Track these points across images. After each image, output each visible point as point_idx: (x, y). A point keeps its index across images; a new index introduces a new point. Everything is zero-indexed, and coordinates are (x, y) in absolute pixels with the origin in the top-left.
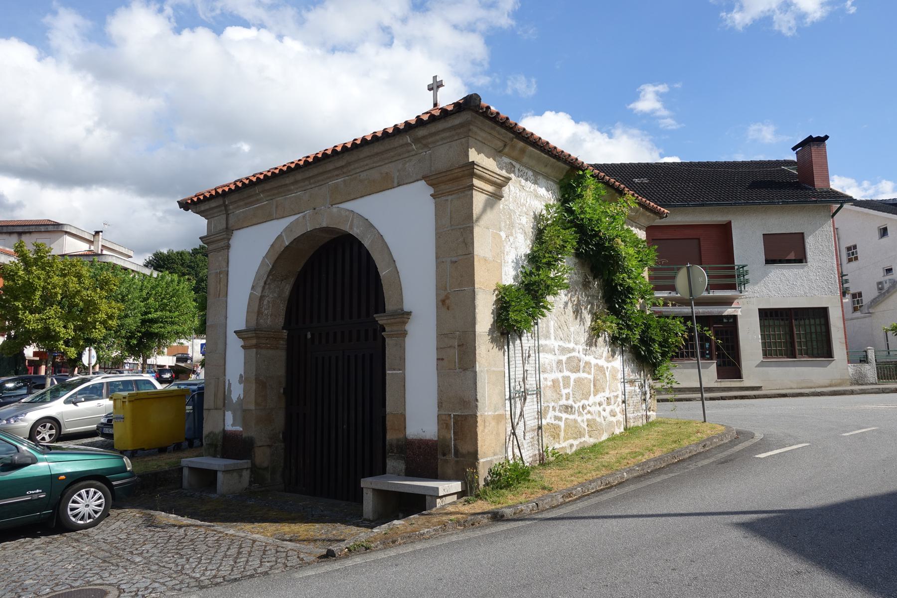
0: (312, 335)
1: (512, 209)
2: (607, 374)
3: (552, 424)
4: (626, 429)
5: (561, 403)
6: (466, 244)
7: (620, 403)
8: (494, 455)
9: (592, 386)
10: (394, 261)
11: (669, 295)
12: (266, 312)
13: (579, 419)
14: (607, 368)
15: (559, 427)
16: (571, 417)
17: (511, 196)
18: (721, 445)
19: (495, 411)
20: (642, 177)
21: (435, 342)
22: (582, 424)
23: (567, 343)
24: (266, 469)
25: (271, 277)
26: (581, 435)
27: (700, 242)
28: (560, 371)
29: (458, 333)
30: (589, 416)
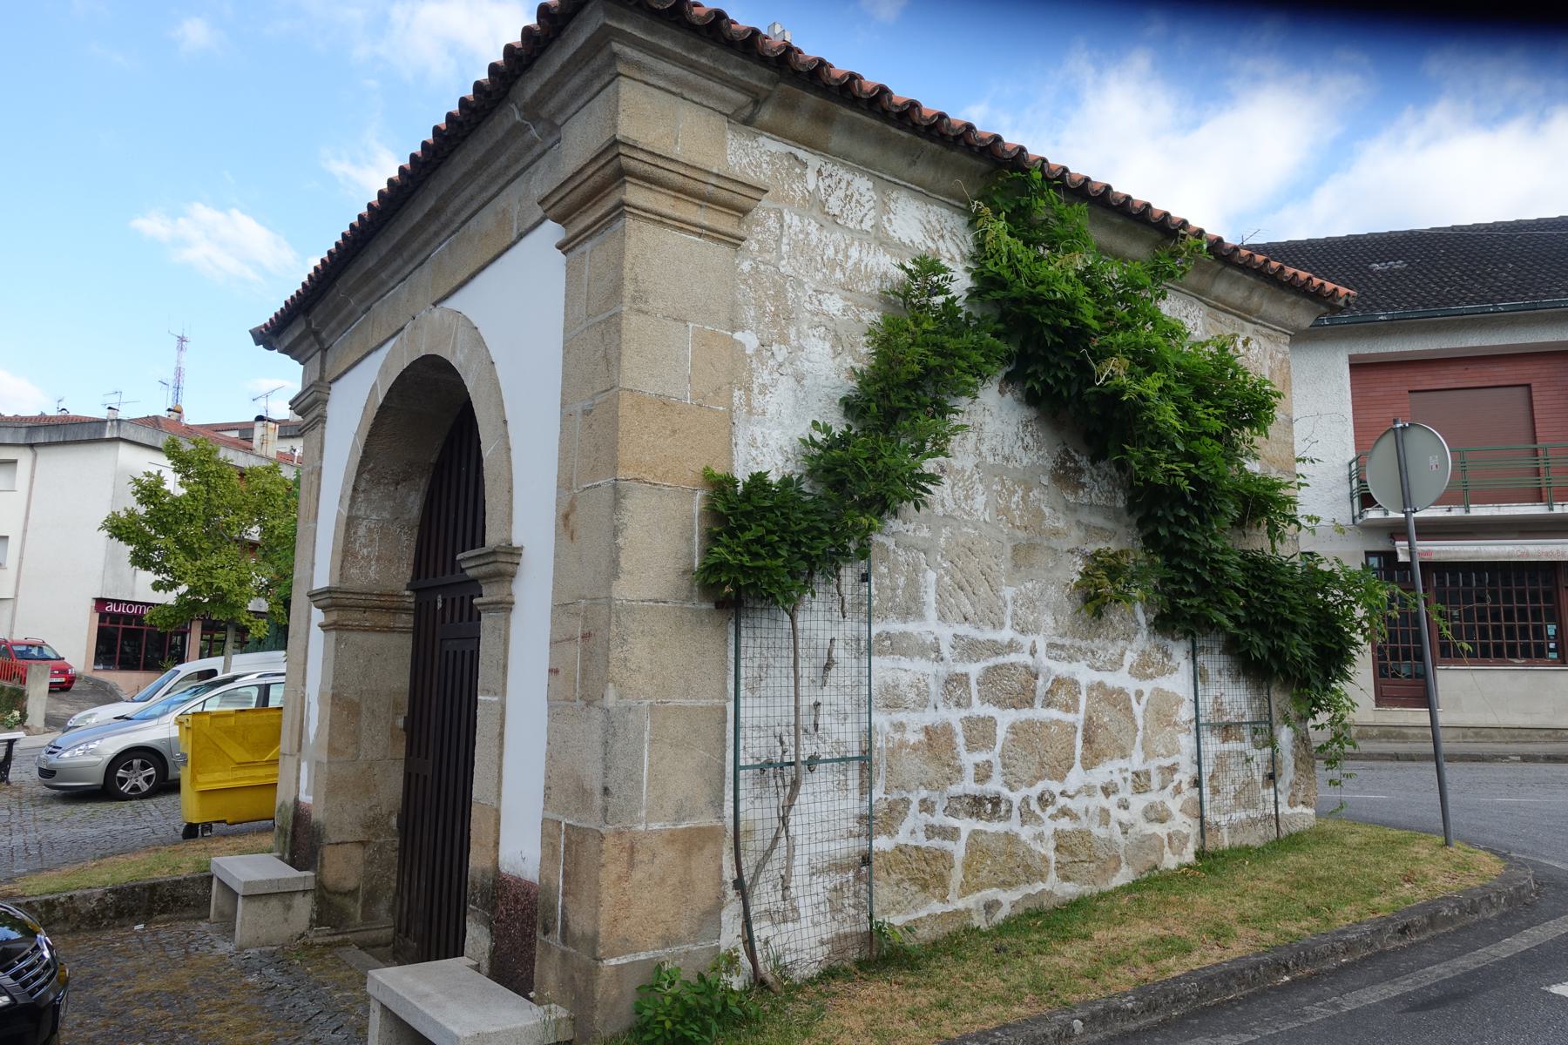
0: (444, 601)
1: (790, 271)
2: (1138, 710)
3: (917, 848)
4: (1200, 854)
5: (956, 789)
6: (608, 363)
7: (1185, 786)
8: (667, 945)
9: (1079, 742)
10: (505, 422)
11: (1448, 514)
12: (365, 551)
13: (1026, 833)
14: (1139, 694)
15: (945, 856)
16: (997, 827)
17: (785, 240)
18: (1466, 928)
19: (679, 820)
20: (1391, 259)
21: (548, 627)
22: (1037, 847)
23: (988, 628)
24: (352, 893)
25: (366, 476)
26: (1032, 872)
27: (1530, 392)
28: (958, 704)
29: (583, 601)
30: (1065, 824)
